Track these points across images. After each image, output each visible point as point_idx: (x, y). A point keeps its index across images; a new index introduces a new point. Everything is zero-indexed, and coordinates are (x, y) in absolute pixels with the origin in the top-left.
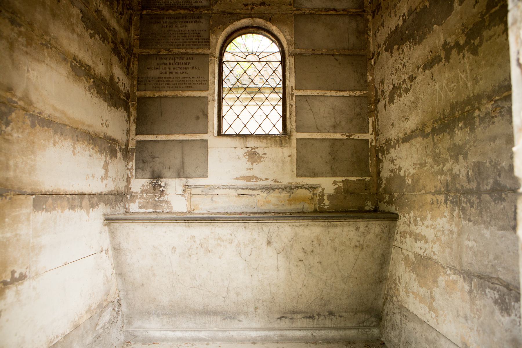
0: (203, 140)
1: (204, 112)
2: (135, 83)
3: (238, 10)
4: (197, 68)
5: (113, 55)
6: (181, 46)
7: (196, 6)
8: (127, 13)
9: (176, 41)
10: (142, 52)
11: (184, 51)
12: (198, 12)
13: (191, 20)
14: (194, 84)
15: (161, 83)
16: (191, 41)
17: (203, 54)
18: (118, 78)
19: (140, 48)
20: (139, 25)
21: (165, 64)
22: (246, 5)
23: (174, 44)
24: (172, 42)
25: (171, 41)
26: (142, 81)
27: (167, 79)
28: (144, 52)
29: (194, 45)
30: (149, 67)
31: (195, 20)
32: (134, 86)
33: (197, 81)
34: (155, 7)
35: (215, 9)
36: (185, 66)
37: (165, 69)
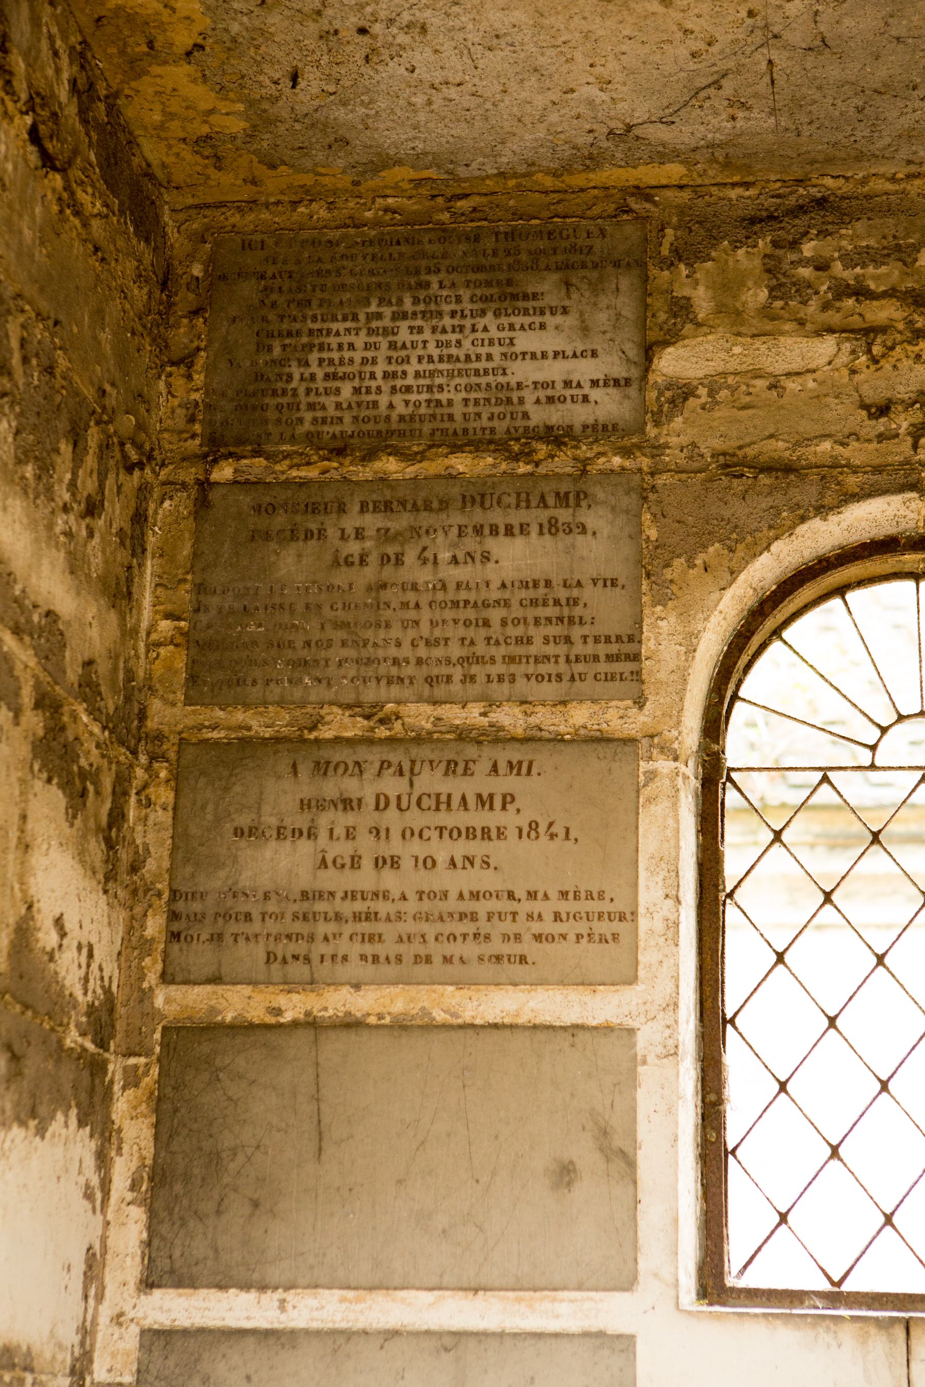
0: (601, 1334)
1: (604, 1133)
2: (154, 926)
3: (826, 445)
4: (558, 829)
5: (38, 785)
6: (456, 687)
7: (550, 428)
8: (119, 488)
9: (422, 652)
10: (200, 727)
11: (473, 715)
12: (563, 463)
13: (516, 518)
14: (538, 938)
15: (323, 928)
16: (520, 650)
17: (601, 740)
18: (59, 922)
19: (188, 701)
20: (186, 550)
21: (347, 804)
22: (883, 410)
23: (408, 670)
24: (396, 662)
25: (393, 652)
26: (199, 918)
27: (359, 906)
28: (214, 728)
29: (540, 678)
30: (244, 820)
31: (544, 515)
32: (145, 947)
33: (557, 917)
34: (293, 439)
35: (673, 440)
36: (477, 818)
37: (350, 834)
